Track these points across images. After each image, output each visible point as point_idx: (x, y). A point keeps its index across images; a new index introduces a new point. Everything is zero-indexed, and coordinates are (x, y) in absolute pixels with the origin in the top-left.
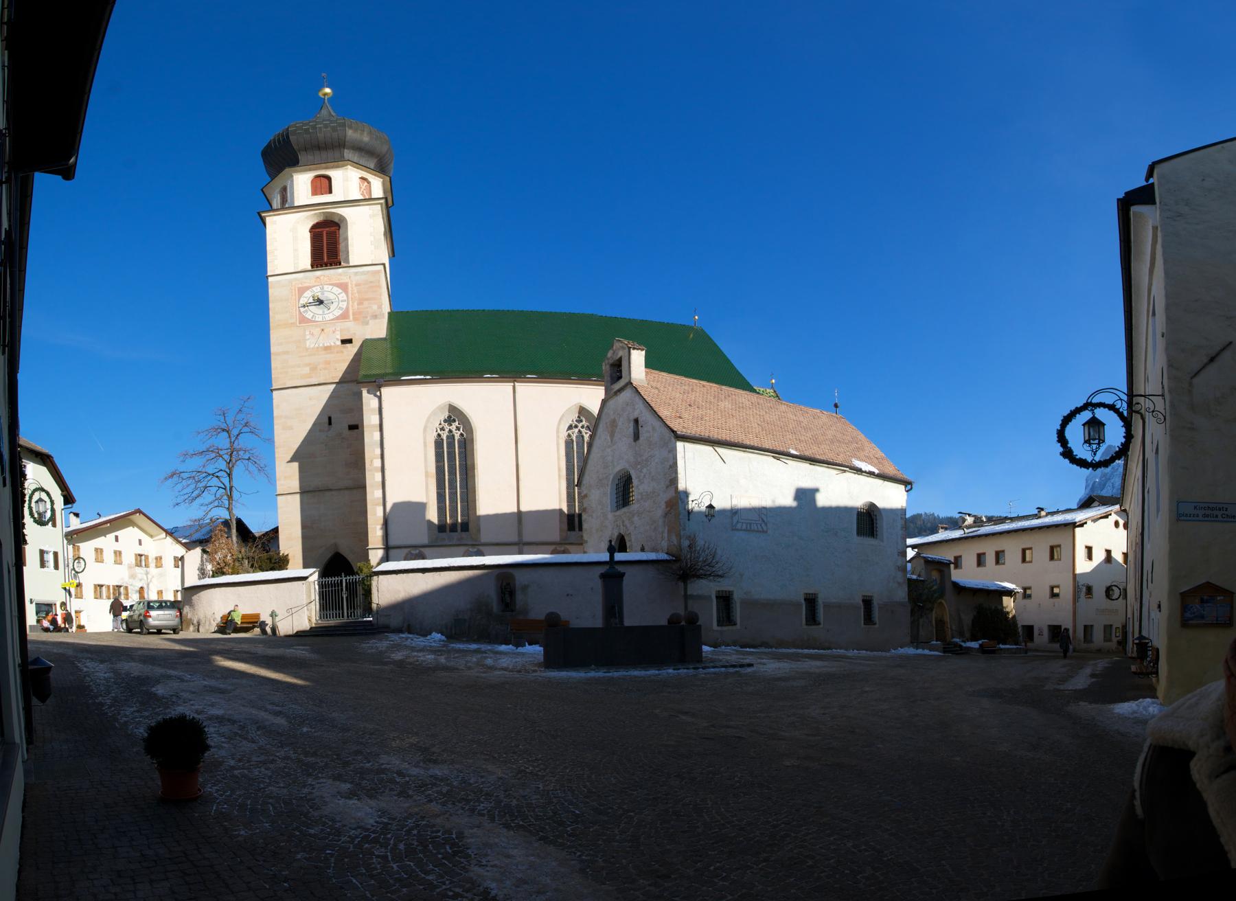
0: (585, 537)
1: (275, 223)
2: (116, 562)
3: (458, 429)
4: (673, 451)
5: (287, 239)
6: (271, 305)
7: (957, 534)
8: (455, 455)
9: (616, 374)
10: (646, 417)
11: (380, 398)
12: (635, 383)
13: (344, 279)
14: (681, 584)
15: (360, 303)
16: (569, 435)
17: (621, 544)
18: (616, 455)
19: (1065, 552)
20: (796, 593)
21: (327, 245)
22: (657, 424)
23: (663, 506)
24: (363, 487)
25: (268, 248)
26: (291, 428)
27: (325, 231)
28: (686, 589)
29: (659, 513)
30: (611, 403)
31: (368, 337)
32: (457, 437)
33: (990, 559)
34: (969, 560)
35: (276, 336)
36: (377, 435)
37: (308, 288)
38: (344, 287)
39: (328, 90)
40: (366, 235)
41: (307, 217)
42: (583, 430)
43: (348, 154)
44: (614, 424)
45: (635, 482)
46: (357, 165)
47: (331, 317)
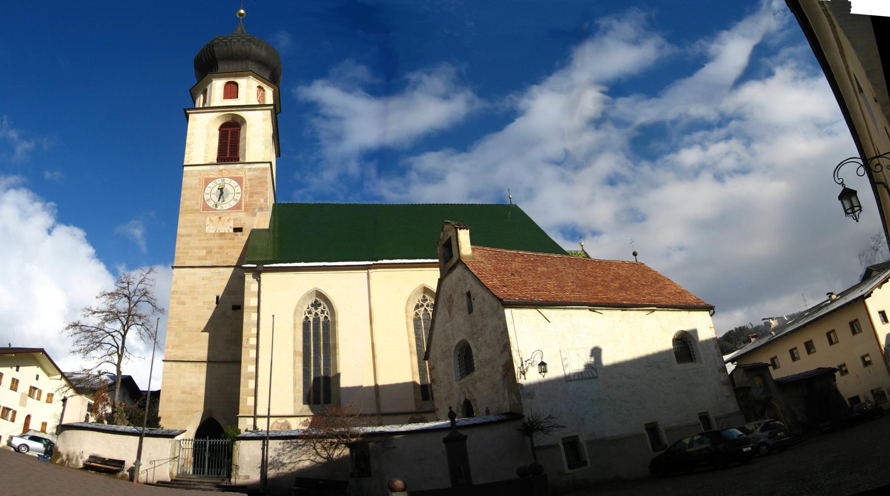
0: (437, 405)
1: (195, 120)
2: (11, 388)
3: (323, 312)
4: (503, 318)
5: (202, 134)
6: (183, 192)
7: (763, 341)
8: (319, 335)
9: (449, 248)
10: (476, 290)
11: (259, 282)
12: (464, 261)
13: (241, 174)
14: (527, 438)
15: (251, 196)
16: (417, 314)
17: (468, 409)
18: (457, 328)
19: (863, 324)
20: (636, 426)
21: (230, 146)
22: (487, 295)
23: (500, 369)
24: (238, 362)
25: (188, 141)
26: (184, 303)
27: (230, 130)
28: (532, 443)
29: (498, 377)
30: (447, 280)
31: (255, 227)
32: (322, 319)
33: (802, 351)
34: (784, 358)
35: (183, 219)
36: (254, 316)
37: (213, 179)
38: (239, 180)
39: (242, 11)
40: (258, 134)
41: (218, 117)
42: (429, 309)
43: (252, 66)
44: (450, 300)
45: (474, 351)
46: (257, 76)
47: (228, 207)
